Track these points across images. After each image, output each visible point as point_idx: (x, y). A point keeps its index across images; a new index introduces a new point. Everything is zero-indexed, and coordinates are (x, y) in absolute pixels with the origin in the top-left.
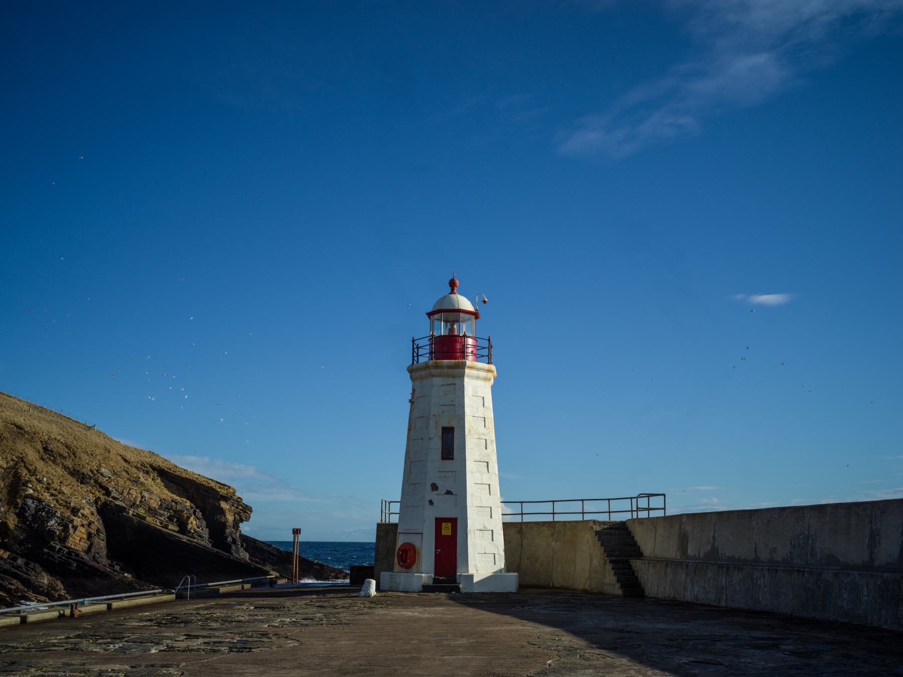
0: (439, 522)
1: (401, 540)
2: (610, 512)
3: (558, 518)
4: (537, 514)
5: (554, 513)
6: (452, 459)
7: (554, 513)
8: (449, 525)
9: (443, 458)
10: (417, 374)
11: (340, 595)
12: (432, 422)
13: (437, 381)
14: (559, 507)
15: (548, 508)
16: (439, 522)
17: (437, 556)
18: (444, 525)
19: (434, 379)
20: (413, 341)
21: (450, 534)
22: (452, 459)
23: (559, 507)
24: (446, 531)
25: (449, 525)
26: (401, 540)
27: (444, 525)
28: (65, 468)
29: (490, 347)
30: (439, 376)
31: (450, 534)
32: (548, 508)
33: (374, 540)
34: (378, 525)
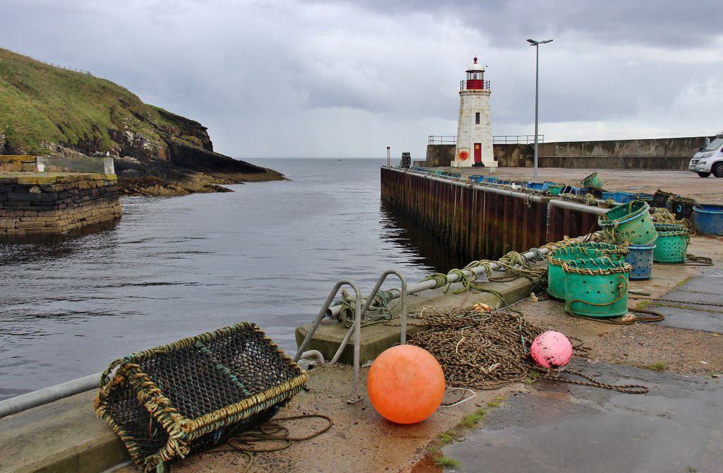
0: (475, 144)
3: (508, 143)
6: (403, 154)
16: (475, 144)
22: (403, 154)
24: (477, 147)
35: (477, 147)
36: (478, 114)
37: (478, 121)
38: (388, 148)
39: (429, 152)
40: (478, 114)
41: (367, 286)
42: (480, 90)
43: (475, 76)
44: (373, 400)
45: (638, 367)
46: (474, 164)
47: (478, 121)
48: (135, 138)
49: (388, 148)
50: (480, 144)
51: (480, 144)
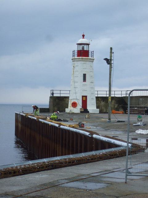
0: (83, 96)
8: (85, 97)
16: (83, 96)
18: (84, 97)
24: (84, 99)
25: (85, 97)
27: (84, 97)
35: (84, 99)
43: (83, 48)
47: (85, 76)
50: (86, 97)
51: (86, 97)
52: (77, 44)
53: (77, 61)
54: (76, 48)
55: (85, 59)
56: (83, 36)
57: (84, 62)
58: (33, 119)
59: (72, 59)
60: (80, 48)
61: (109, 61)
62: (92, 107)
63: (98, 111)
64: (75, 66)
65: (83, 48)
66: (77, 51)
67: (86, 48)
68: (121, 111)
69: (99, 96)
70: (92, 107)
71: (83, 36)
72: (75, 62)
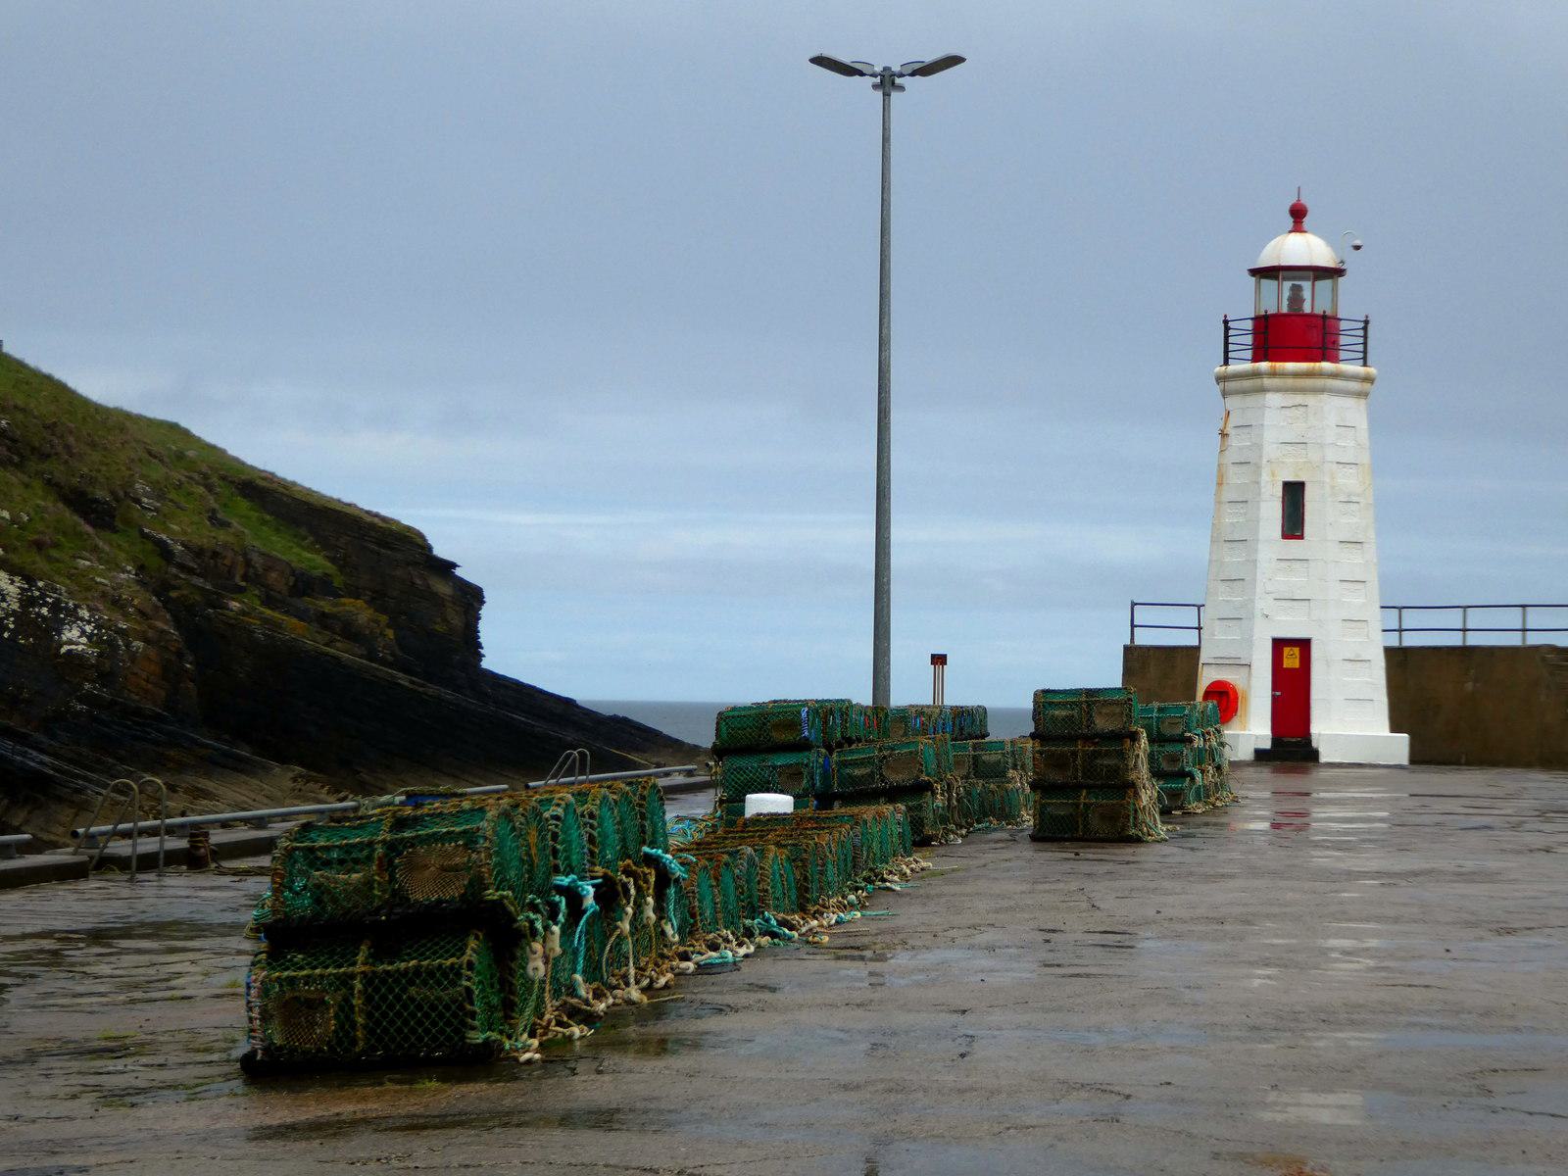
0: (1279, 644)
1: (1206, 677)
2: (1524, 630)
3: (1473, 640)
4: (1434, 632)
5: (1401, 630)
6: (1301, 537)
7: (1401, 630)
8: (1297, 650)
9: (1285, 536)
10: (1232, 385)
11: (421, 1121)
12: (1265, 477)
13: (1274, 399)
14: (1475, 619)
15: (1454, 619)
16: (1279, 644)
17: (1275, 699)
18: (1286, 650)
19: (1269, 396)
20: (1226, 322)
21: (1297, 665)
22: (1301, 537)
23: (1475, 619)
24: (1291, 660)
25: (1297, 650)
26: (1206, 677)
27: (1286, 650)
28: (51, 484)
29: (1365, 329)
30: (1277, 390)
31: (1297, 665)
32: (1454, 619)
33: (1118, 684)
34: (1127, 649)
35: (1291, 660)
36: (1294, 492)
37: (1293, 525)
38: (939, 660)
39: (1035, 702)
40: (1294, 492)
41: (185, 967)
42: (1326, 365)
43: (1296, 298)
44: (271, 1087)
45: (150, 453)
46: (1267, 745)
47: (1293, 525)
48: (27, 601)
49: (939, 660)
50: (1304, 645)
51: (1304, 645)
52: (1254, 272)
53: (1244, 392)
54: (1246, 302)
55: (1296, 375)
56: (1298, 214)
57: (1299, 399)
58: (567, 905)
59: (1221, 379)
60: (1274, 299)
61: (964, 1012)
62: (1353, 719)
63: (1399, 747)
64: (1228, 430)
65: (1296, 298)
66: (1249, 325)
67: (1315, 299)
68: (257, 560)
69: (1411, 640)
70: (1353, 719)
71: (1298, 214)
72: (1233, 402)
